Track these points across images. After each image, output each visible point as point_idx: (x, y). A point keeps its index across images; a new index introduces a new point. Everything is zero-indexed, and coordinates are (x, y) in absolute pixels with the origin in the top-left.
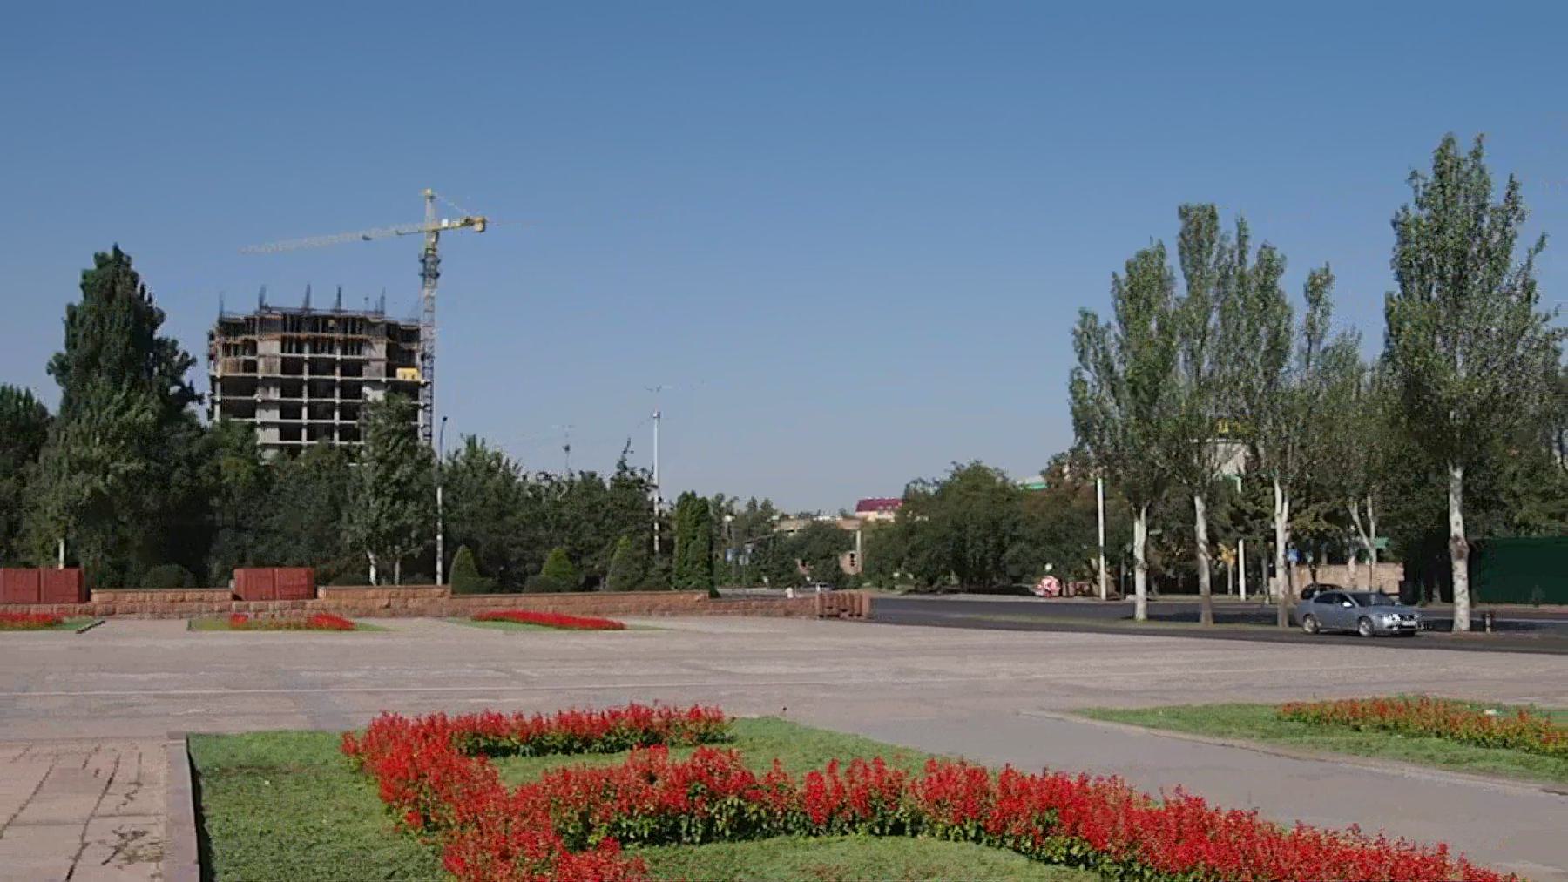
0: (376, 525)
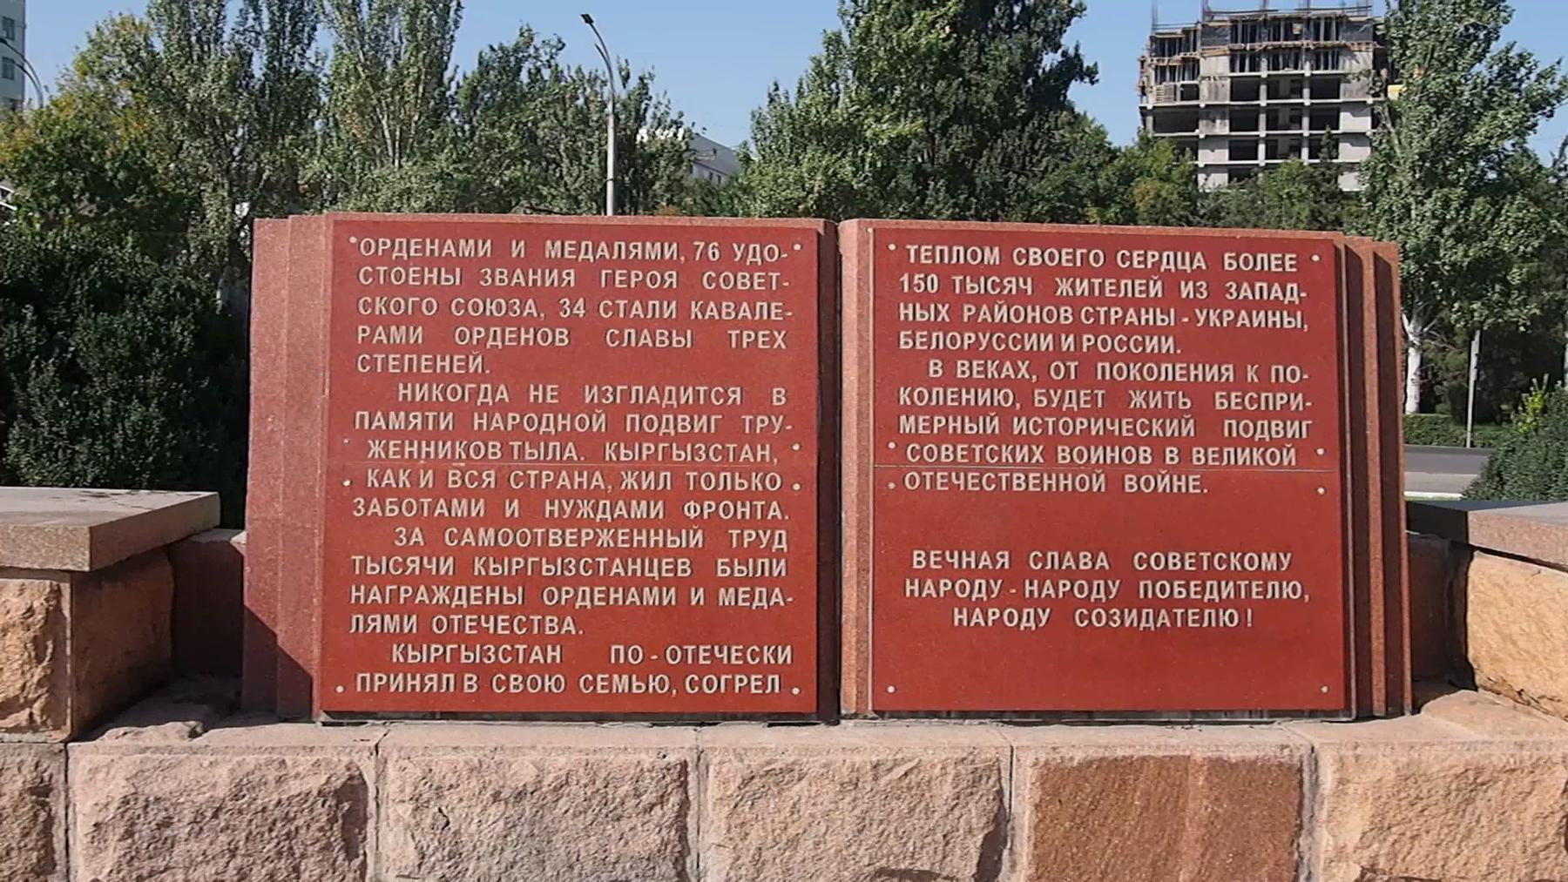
0: (1433, 249)
